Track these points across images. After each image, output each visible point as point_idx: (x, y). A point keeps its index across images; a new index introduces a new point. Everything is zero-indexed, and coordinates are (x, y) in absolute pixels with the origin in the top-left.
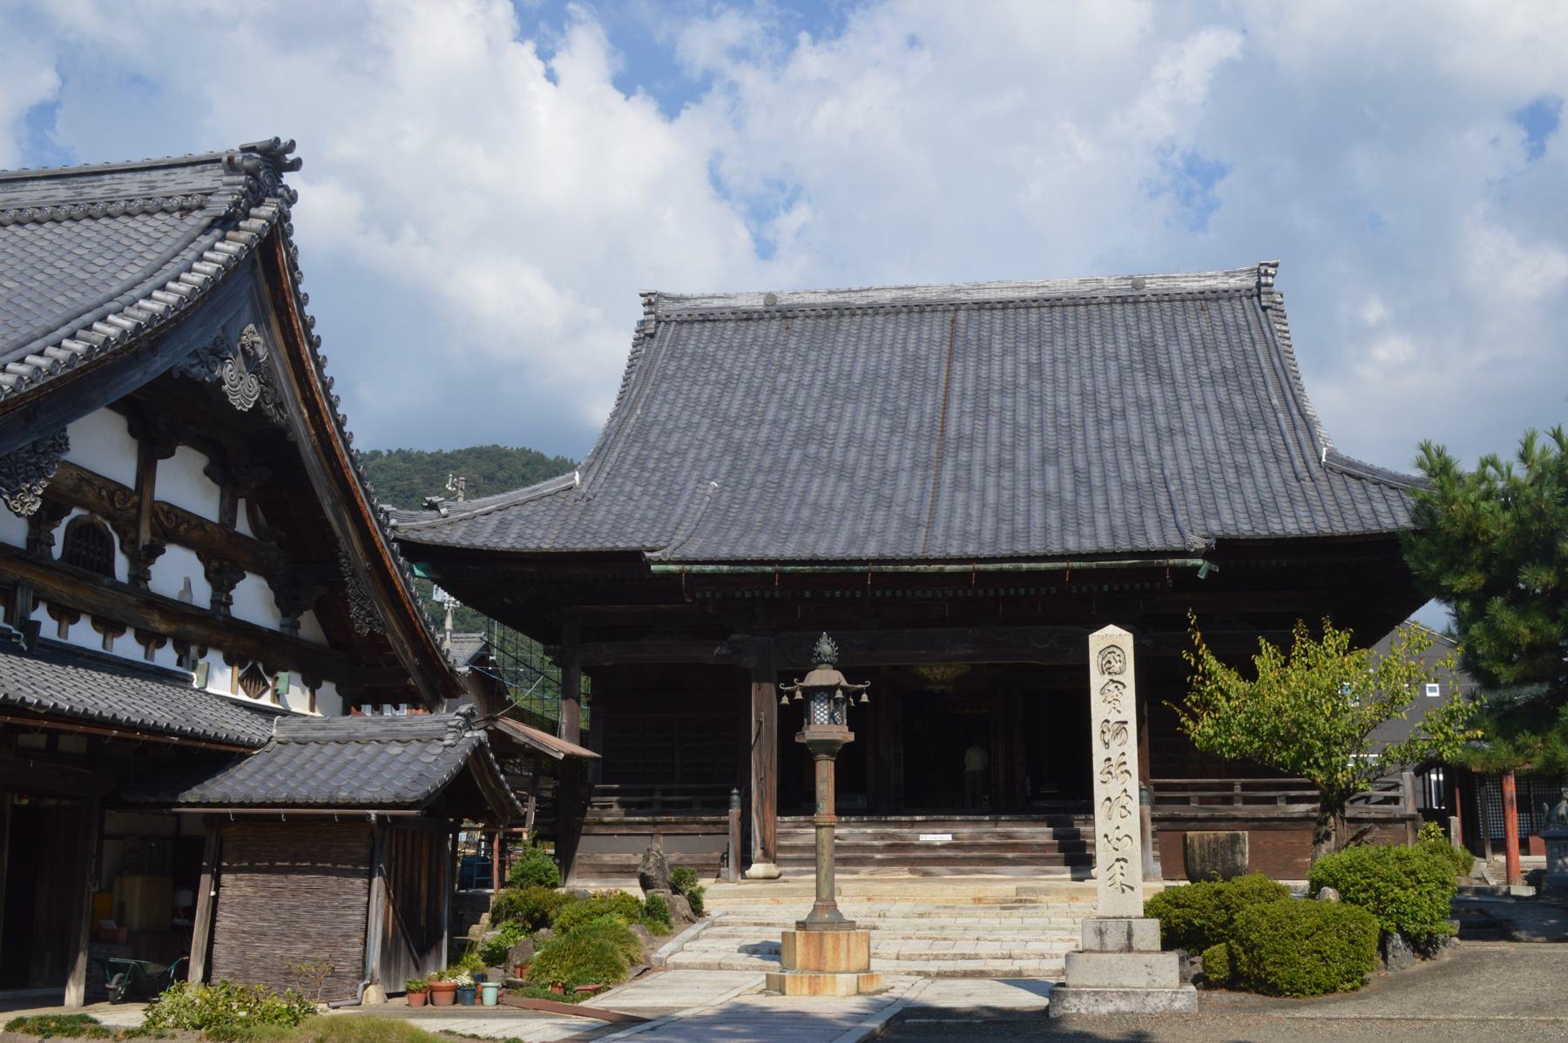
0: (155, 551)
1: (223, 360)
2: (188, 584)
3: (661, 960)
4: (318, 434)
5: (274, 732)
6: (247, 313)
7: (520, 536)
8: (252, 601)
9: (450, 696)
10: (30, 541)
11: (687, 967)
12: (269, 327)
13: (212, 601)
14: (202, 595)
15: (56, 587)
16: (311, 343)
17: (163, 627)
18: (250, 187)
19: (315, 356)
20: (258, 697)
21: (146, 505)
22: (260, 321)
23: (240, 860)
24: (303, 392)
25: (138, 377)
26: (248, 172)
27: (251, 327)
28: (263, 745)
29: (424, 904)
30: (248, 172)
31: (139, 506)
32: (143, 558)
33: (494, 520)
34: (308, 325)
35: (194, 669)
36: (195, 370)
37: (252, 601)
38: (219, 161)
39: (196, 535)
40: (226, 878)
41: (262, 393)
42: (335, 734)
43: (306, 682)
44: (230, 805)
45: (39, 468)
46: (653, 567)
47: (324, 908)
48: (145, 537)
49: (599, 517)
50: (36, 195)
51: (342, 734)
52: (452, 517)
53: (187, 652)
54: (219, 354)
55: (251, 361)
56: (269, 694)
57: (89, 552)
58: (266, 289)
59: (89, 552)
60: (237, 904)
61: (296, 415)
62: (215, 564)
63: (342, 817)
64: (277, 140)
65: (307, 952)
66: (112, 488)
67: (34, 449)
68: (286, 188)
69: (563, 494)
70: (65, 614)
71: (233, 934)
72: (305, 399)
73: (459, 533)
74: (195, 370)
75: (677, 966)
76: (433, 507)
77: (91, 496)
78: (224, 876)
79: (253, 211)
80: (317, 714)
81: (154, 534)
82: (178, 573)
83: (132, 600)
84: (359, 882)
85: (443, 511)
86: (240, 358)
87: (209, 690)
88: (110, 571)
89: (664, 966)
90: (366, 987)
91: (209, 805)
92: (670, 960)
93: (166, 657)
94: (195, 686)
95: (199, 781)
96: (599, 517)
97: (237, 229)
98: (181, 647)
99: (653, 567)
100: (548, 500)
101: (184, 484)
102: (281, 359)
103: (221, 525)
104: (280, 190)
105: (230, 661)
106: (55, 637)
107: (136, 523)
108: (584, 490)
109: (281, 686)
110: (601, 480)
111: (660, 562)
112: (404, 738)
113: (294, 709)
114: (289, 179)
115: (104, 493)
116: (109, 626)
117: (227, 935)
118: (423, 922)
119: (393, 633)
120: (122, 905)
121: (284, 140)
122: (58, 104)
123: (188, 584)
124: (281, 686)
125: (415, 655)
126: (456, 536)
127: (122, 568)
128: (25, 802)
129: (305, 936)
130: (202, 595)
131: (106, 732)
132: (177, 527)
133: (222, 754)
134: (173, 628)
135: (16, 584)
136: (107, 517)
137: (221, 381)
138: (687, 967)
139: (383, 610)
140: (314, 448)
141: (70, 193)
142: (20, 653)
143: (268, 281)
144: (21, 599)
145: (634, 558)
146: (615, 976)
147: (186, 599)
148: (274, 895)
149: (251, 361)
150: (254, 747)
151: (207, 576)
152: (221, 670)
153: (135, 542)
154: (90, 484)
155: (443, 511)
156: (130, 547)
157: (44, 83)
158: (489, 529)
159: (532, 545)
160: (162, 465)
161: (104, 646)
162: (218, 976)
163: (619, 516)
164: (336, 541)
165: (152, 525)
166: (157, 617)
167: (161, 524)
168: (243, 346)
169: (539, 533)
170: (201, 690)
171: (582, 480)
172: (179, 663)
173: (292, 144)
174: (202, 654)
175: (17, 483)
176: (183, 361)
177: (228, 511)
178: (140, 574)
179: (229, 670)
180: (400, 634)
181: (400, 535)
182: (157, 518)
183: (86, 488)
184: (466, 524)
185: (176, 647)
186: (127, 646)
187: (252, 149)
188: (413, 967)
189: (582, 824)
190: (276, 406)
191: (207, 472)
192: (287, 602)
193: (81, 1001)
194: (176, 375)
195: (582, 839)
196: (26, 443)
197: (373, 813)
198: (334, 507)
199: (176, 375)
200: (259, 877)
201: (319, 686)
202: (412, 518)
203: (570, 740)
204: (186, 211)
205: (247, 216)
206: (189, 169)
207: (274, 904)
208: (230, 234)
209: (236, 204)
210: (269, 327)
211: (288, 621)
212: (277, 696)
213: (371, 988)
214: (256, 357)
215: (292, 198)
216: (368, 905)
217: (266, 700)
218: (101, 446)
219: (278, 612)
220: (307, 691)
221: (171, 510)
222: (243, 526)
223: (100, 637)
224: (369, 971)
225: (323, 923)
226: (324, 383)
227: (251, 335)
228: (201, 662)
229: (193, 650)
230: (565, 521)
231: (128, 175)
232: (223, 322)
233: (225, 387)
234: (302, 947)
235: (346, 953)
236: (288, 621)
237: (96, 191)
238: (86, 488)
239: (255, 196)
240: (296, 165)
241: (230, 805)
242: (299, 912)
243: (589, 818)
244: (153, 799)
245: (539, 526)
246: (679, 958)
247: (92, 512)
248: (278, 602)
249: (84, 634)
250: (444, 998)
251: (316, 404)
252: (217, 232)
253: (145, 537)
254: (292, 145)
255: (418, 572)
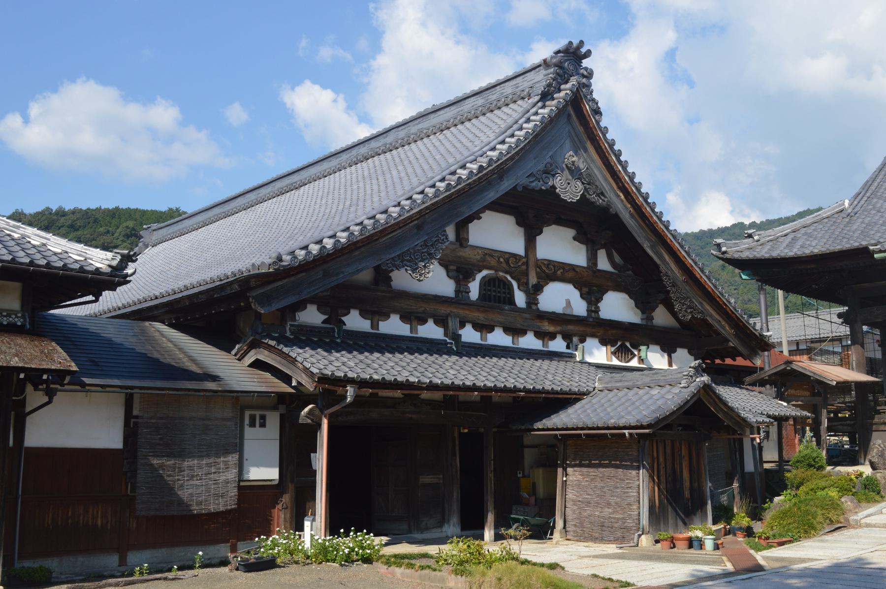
0: (539, 288)
1: (554, 176)
2: (568, 303)
3: (856, 521)
4: (633, 206)
5: (597, 384)
6: (568, 143)
7: (802, 247)
8: (617, 306)
9: (764, 350)
10: (457, 292)
11: (875, 526)
12: (586, 150)
13: (587, 311)
14: (580, 308)
15: (480, 317)
16: (615, 155)
17: (551, 329)
18: (558, 74)
19: (620, 162)
20: (628, 362)
21: (532, 263)
22: (577, 148)
23: (575, 460)
24: (617, 184)
25: (492, 194)
26: (556, 65)
27: (571, 153)
28: (590, 392)
29: (687, 484)
30: (556, 65)
31: (527, 263)
32: (533, 293)
33: (788, 239)
34: (612, 144)
35: (576, 350)
36: (534, 184)
37: (617, 306)
38: (540, 66)
39: (570, 274)
40: (569, 470)
41: (586, 189)
42: (626, 384)
43: (663, 350)
44: (558, 429)
45: (430, 254)
46: (876, 256)
47: (617, 488)
48: (533, 280)
49: (855, 227)
50: (470, 106)
51: (630, 384)
52: (762, 240)
53: (571, 341)
54: (549, 172)
55: (575, 172)
56: (636, 359)
57: (496, 295)
58: (581, 129)
59: (496, 295)
60: (575, 484)
61: (614, 198)
62: (585, 290)
63: (587, 435)
64: (571, 43)
65: (611, 513)
66: (507, 256)
67: (425, 244)
68: (586, 69)
69: (836, 216)
70: (484, 328)
71: (575, 502)
72: (619, 188)
73: (766, 250)
74: (534, 184)
75: (868, 525)
76: (750, 236)
77: (493, 262)
78: (568, 469)
79: (563, 87)
80: (675, 367)
81: (539, 277)
82: (559, 297)
83: (527, 316)
84: (634, 472)
85: (756, 238)
86: (566, 172)
87: (589, 359)
88: (511, 301)
89: (858, 525)
90: (640, 536)
91: (548, 429)
92: (863, 521)
93: (558, 345)
94: (578, 359)
95: (548, 415)
96: (855, 227)
97: (553, 99)
98: (567, 337)
99: (876, 256)
100: (826, 220)
101: (558, 245)
102: (597, 167)
103: (588, 267)
104: (582, 71)
105: (604, 342)
106: (479, 341)
107: (526, 274)
108: (849, 211)
109: (643, 354)
110: (862, 202)
111: (880, 251)
112: (661, 384)
113: (655, 367)
114: (585, 63)
115: (502, 260)
116: (515, 331)
117: (571, 503)
118: (687, 494)
119: (711, 316)
120: (534, 484)
121: (575, 43)
122: (676, 49)
123: (568, 303)
124: (643, 354)
125: (732, 328)
126: (763, 253)
127: (520, 299)
128: (466, 431)
129: (609, 504)
130: (580, 308)
131: (471, 394)
132: (555, 272)
133: (561, 400)
134: (559, 328)
135: (447, 316)
136: (506, 272)
137: (554, 187)
138: (875, 526)
139: (701, 304)
140: (631, 215)
141: (483, 101)
142: (450, 353)
143: (581, 124)
144: (452, 323)
145: (863, 252)
146: (806, 532)
147: (568, 312)
148: (592, 480)
149: (575, 172)
150: (584, 394)
151: (582, 296)
152: (598, 348)
153: (527, 284)
154: (492, 256)
155: (756, 238)
156: (524, 286)
157: (670, 37)
158: (784, 245)
159: (807, 252)
160: (539, 239)
161: (513, 343)
162: (570, 528)
163: (868, 225)
164: (657, 266)
165: (537, 273)
166: (547, 324)
167: (544, 272)
168: (567, 167)
169: (814, 244)
170: (582, 362)
171: (850, 205)
172: (568, 347)
173: (582, 43)
174: (583, 341)
175: (416, 264)
176: (524, 181)
177: (592, 258)
178: (532, 301)
179: (604, 348)
180: (717, 316)
181: (728, 256)
182: (540, 267)
183: (488, 258)
184: (771, 243)
185: (564, 338)
186: (529, 341)
187: (558, 52)
188: (680, 523)
189: (872, 424)
190: (598, 195)
191: (575, 238)
192: (644, 304)
193: (493, 538)
194: (520, 189)
195: (874, 433)
196: (419, 242)
197: (626, 432)
198: (652, 247)
199: (520, 189)
200: (585, 470)
201: (675, 351)
202: (736, 245)
203: (859, 370)
204: (529, 96)
205: (559, 91)
206: (533, 72)
207: (593, 485)
208: (548, 103)
209: (550, 85)
210: (586, 150)
211: (645, 316)
212: (641, 360)
213: (643, 537)
214: (578, 169)
215: (590, 75)
216: (638, 487)
217: (634, 363)
218: (497, 234)
219: (639, 311)
220: (666, 356)
221: (549, 263)
222: (604, 264)
223: (510, 338)
224: (641, 526)
225: (617, 497)
226: (629, 177)
227: (570, 157)
228: (580, 346)
229: (575, 339)
230: (833, 233)
231: (507, 84)
232: (551, 153)
233: (557, 190)
234: (607, 511)
235: (630, 515)
236: (645, 316)
237: (493, 96)
238: (488, 258)
239: (562, 77)
240: (588, 54)
241: (558, 429)
242: (605, 490)
243: (876, 420)
244: (523, 427)
245: (815, 239)
246: (868, 520)
247: (496, 271)
248: (637, 306)
249: (498, 338)
250: (681, 546)
251: (627, 189)
252: (540, 104)
253: (533, 280)
254: (582, 43)
255: (744, 277)
